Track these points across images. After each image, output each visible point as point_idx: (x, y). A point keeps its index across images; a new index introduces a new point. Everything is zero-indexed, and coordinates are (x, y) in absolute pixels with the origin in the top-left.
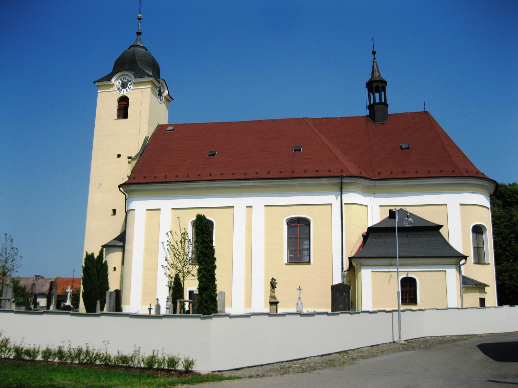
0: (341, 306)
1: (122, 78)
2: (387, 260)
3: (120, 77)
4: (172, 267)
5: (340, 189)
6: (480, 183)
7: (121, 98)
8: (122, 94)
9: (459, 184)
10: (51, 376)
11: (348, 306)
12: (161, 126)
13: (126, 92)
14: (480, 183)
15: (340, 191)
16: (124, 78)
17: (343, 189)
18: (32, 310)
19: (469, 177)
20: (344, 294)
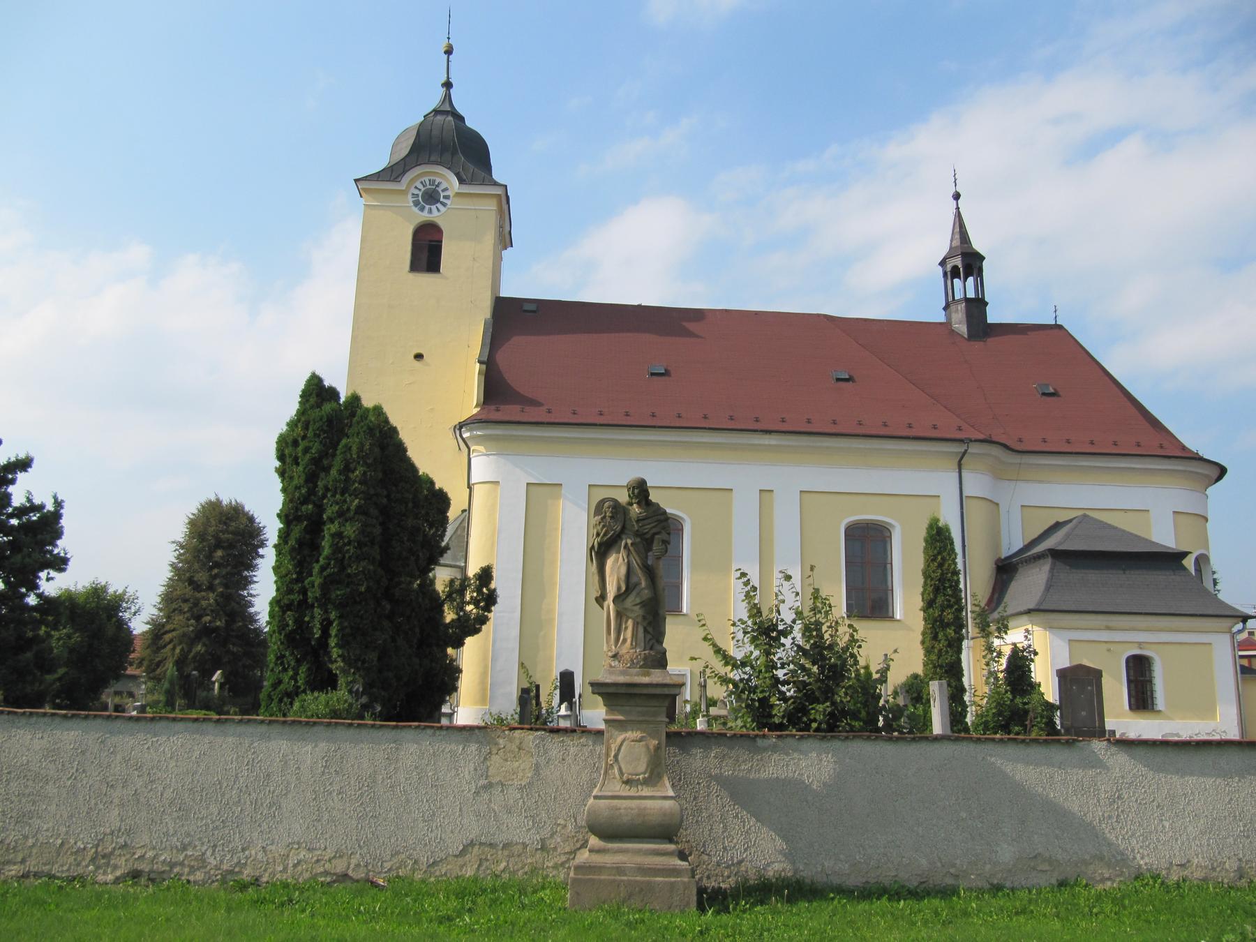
0: (1084, 713)
1: (427, 179)
2: (1100, 617)
3: (422, 177)
4: (488, 609)
5: (956, 467)
6: (1180, 468)
7: (422, 226)
8: (424, 216)
9: (769, 448)
10: (559, 843)
11: (1098, 715)
12: (756, 314)
13: (434, 214)
14: (1180, 468)
15: (957, 470)
16: (430, 181)
17: (962, 466)
18: (1062, 735)
19: (705, 428)
20: (1089, 688)
